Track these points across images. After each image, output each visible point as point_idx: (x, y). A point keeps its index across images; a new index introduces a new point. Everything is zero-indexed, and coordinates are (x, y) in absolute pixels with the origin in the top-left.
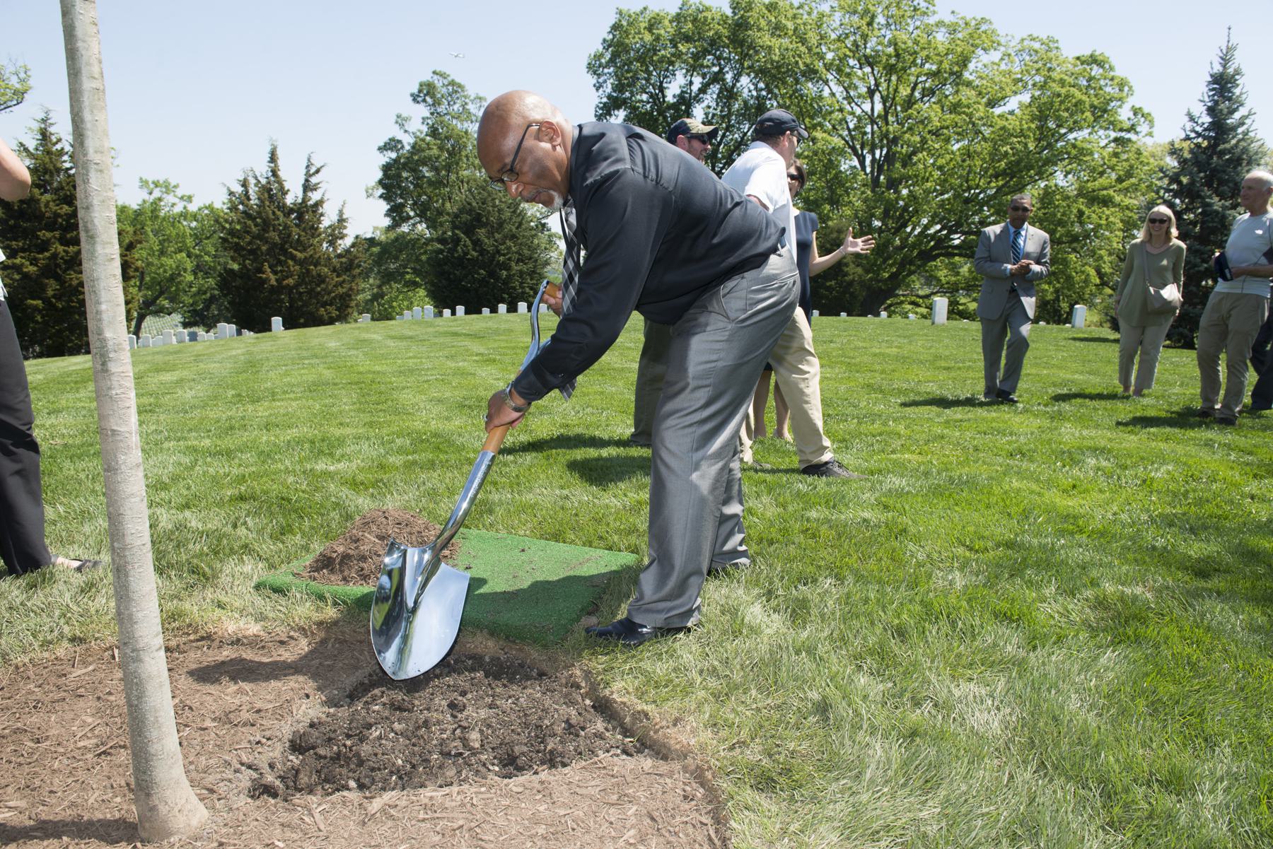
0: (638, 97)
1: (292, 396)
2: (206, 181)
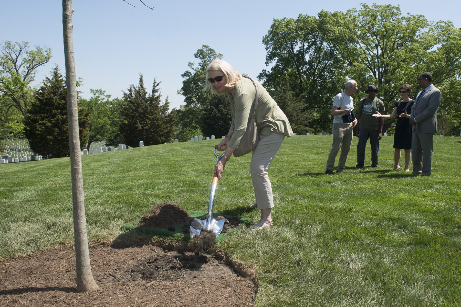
1: (143, 169)
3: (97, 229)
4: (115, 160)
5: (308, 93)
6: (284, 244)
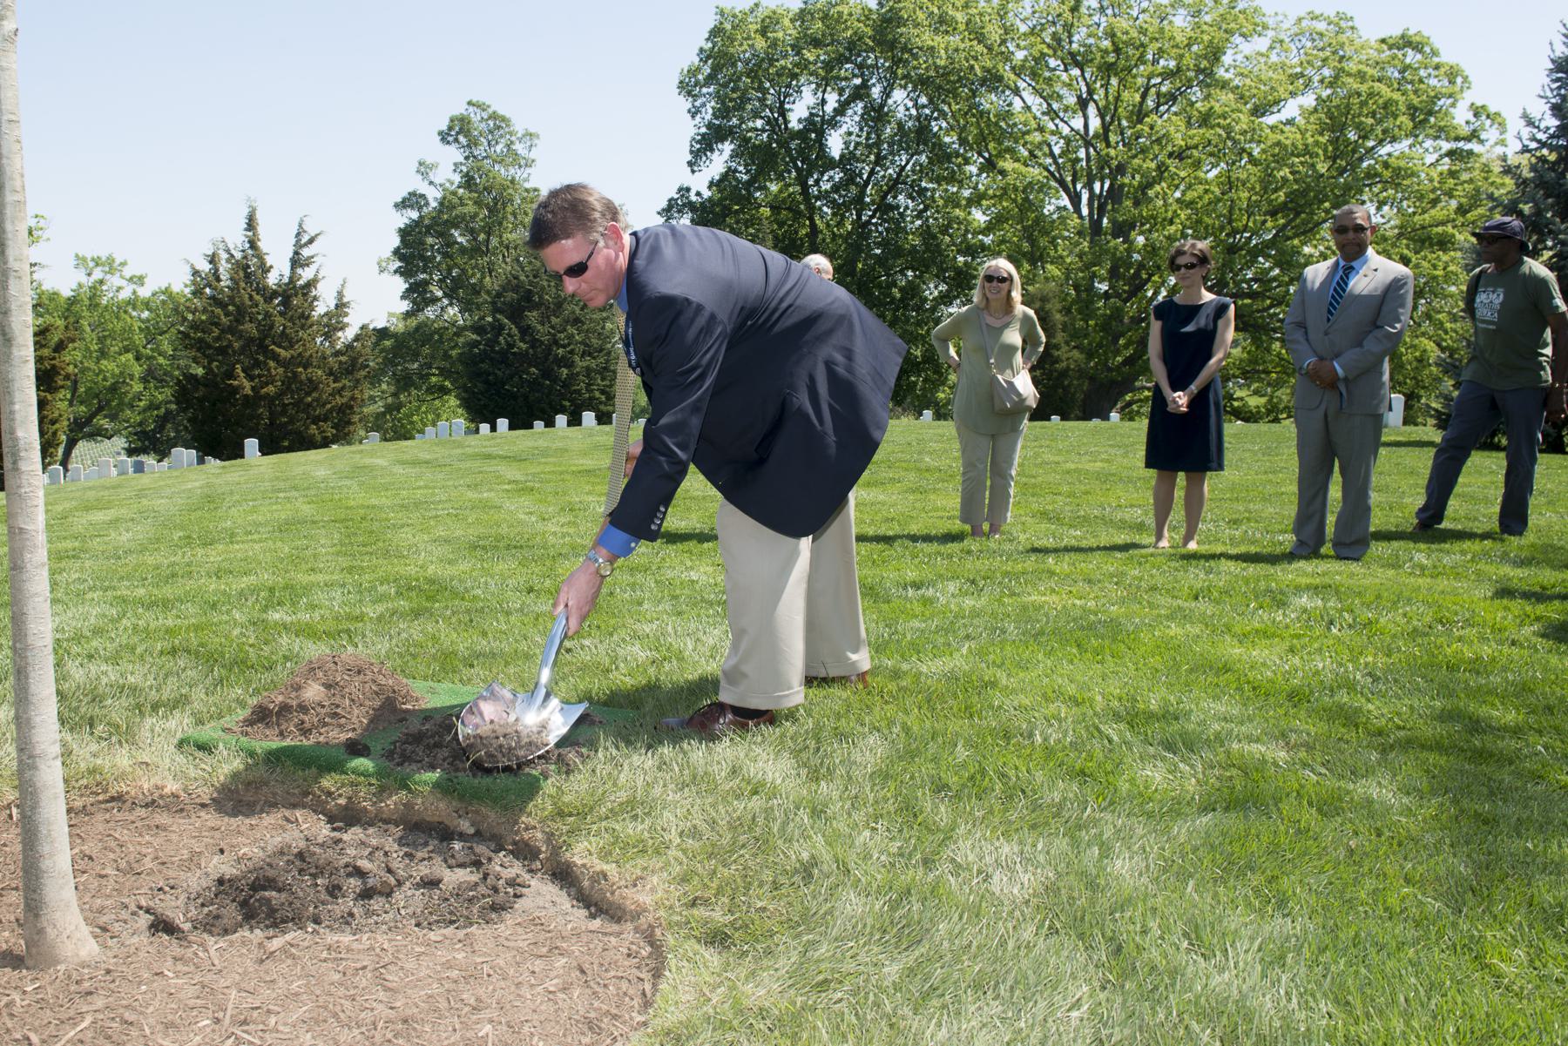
0: (751, 124)
1: (255, 537)
3: (94, 747)
4: (160, 503)
6: (756, 803)
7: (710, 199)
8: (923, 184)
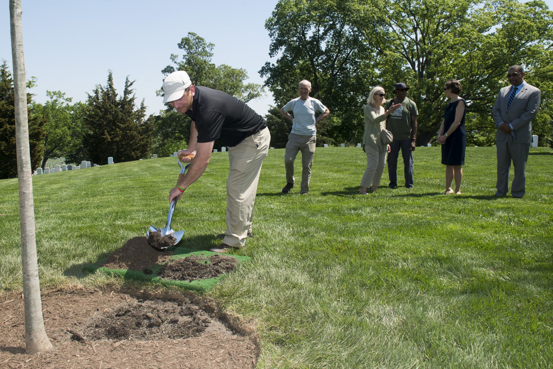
0: (292, 39)
1: (111, 193)
2: (78, 92)
3: (52, 271)
5: (325, 92)
6: (294, 291)
7: (277, 67)
8: (356, 60)
